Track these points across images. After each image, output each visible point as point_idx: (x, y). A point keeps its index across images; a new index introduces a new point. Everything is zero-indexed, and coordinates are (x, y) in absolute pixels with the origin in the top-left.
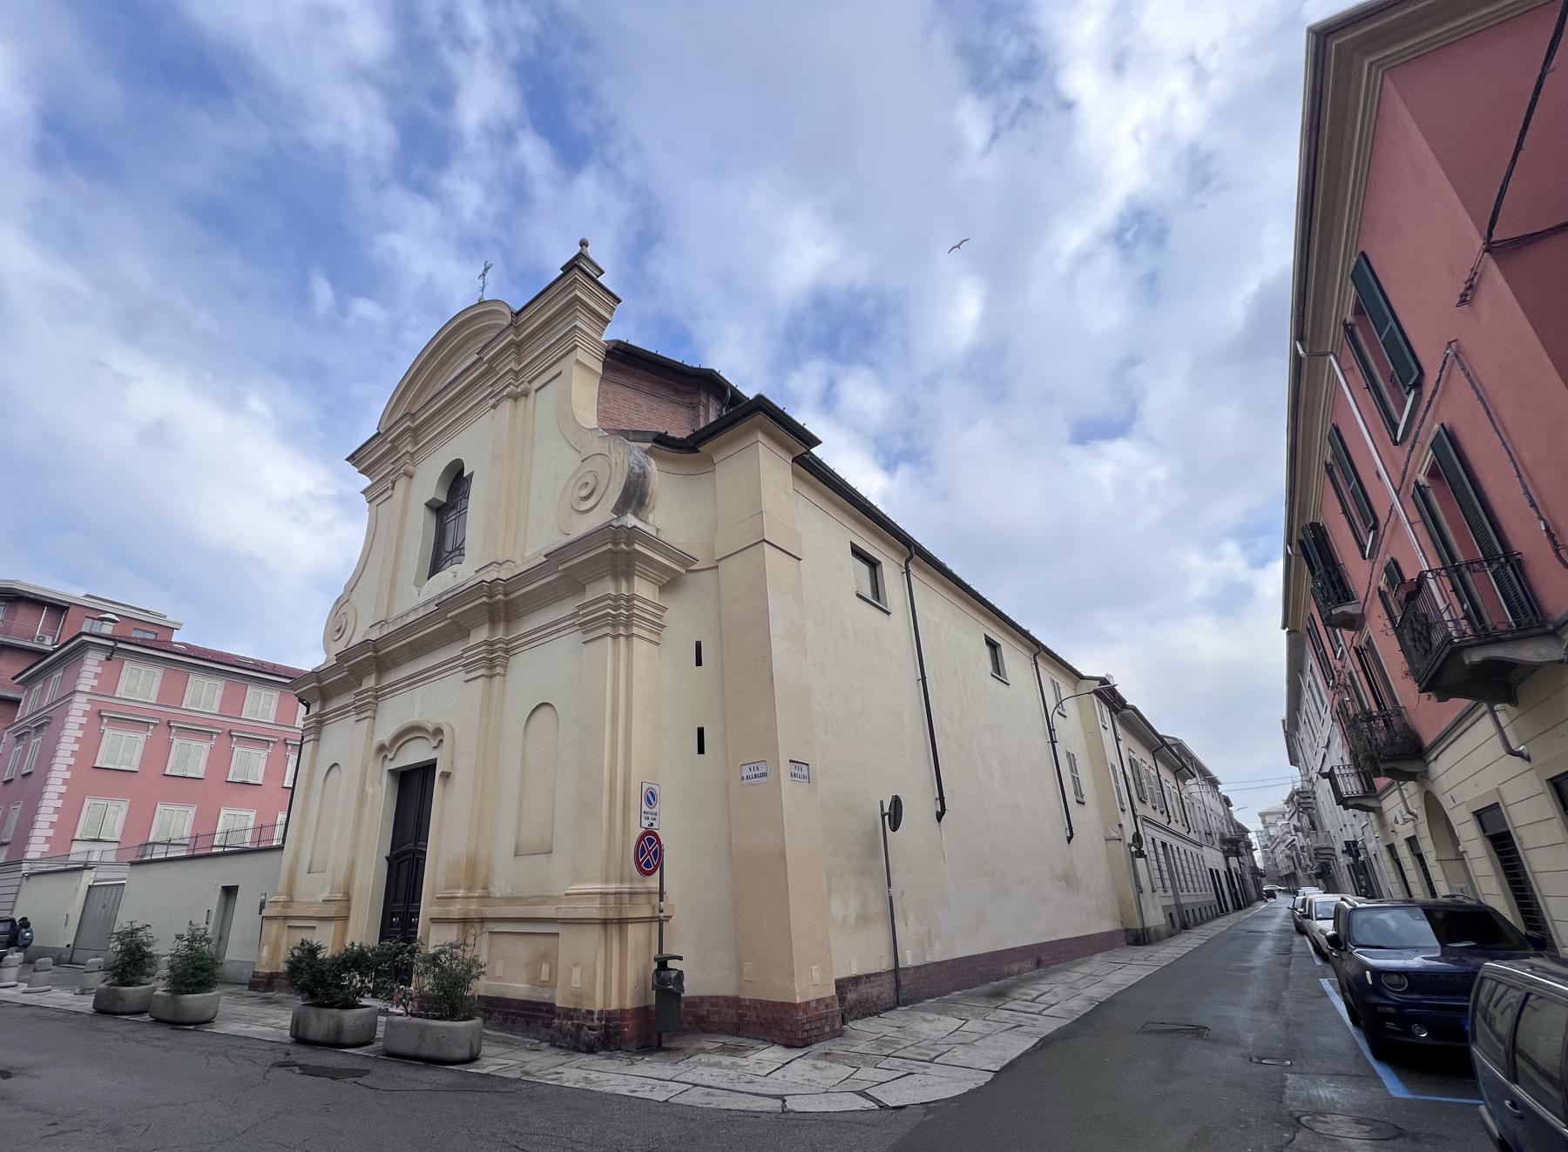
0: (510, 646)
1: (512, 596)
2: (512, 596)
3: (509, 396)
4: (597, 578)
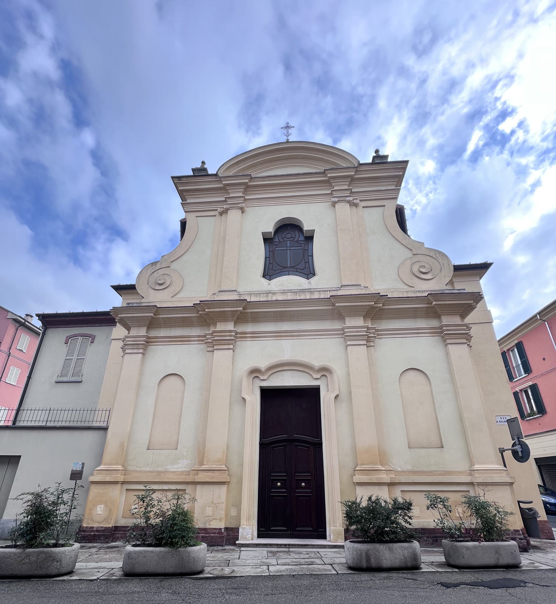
0: (149, 340)
1: (386, 307)
2: (386, 307)
3: (349, 202)
4: (139, 326)
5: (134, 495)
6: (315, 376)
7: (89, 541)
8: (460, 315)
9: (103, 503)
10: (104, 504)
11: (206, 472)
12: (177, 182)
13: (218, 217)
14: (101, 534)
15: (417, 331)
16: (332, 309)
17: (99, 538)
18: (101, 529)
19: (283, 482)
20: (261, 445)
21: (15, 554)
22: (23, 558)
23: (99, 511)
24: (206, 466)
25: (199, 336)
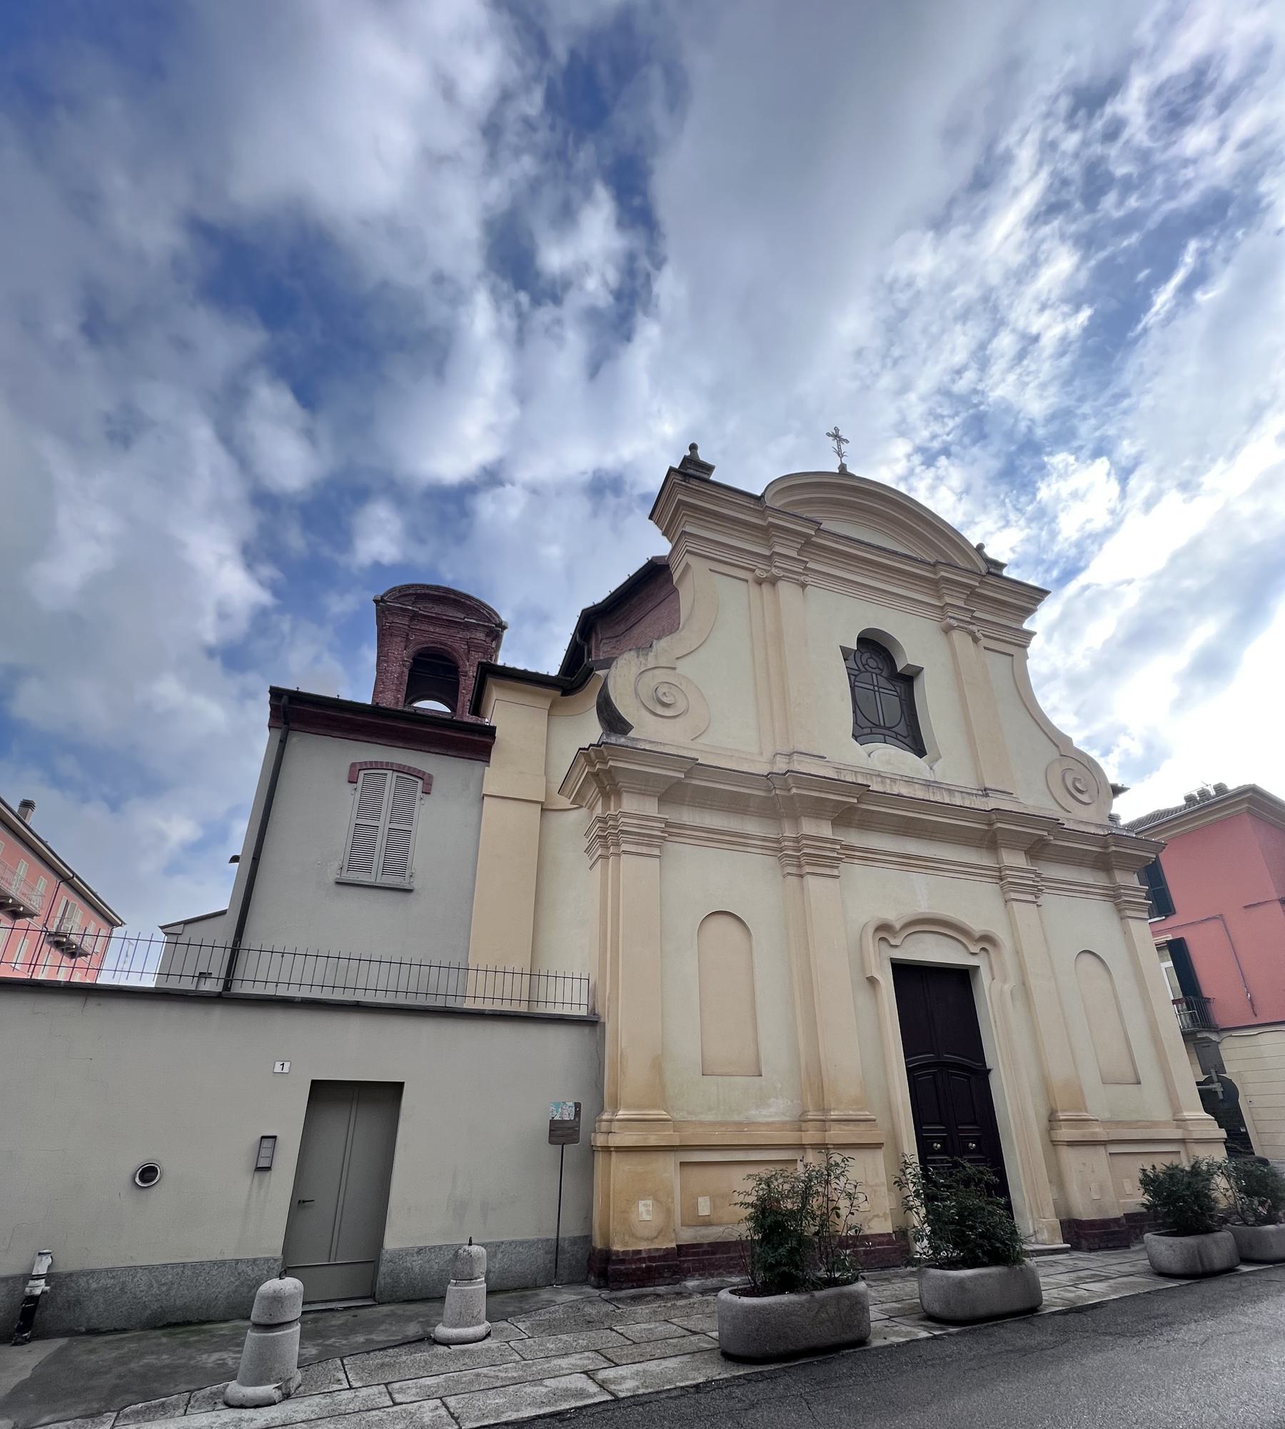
4: (643, 793)
5: (1162, 1164)
6: (975, 949)
7: (639, 1283)
8: (1025, 851)
9: (649, 1195)
10: (651, 1197)
11: (844, 1125)
12: (680, 482)
13: (754, 589)
14: (662, 1265)
15: (736, 841)
16: (987, 831)
17: (660, 1274)
18: (657, 1254)
19: (942, 1140)
20: (907, 1069)
21: (802, 1304)
22: (817, 1310)
23: (644, 1214)
24: (836, 1113)
25: (765, 839)
